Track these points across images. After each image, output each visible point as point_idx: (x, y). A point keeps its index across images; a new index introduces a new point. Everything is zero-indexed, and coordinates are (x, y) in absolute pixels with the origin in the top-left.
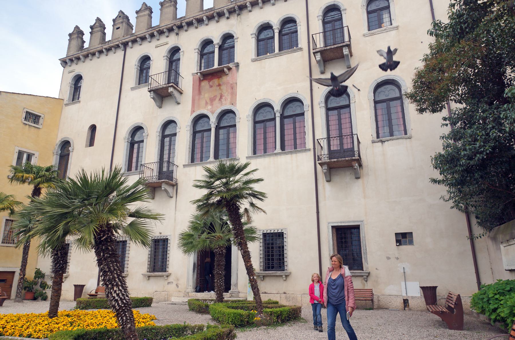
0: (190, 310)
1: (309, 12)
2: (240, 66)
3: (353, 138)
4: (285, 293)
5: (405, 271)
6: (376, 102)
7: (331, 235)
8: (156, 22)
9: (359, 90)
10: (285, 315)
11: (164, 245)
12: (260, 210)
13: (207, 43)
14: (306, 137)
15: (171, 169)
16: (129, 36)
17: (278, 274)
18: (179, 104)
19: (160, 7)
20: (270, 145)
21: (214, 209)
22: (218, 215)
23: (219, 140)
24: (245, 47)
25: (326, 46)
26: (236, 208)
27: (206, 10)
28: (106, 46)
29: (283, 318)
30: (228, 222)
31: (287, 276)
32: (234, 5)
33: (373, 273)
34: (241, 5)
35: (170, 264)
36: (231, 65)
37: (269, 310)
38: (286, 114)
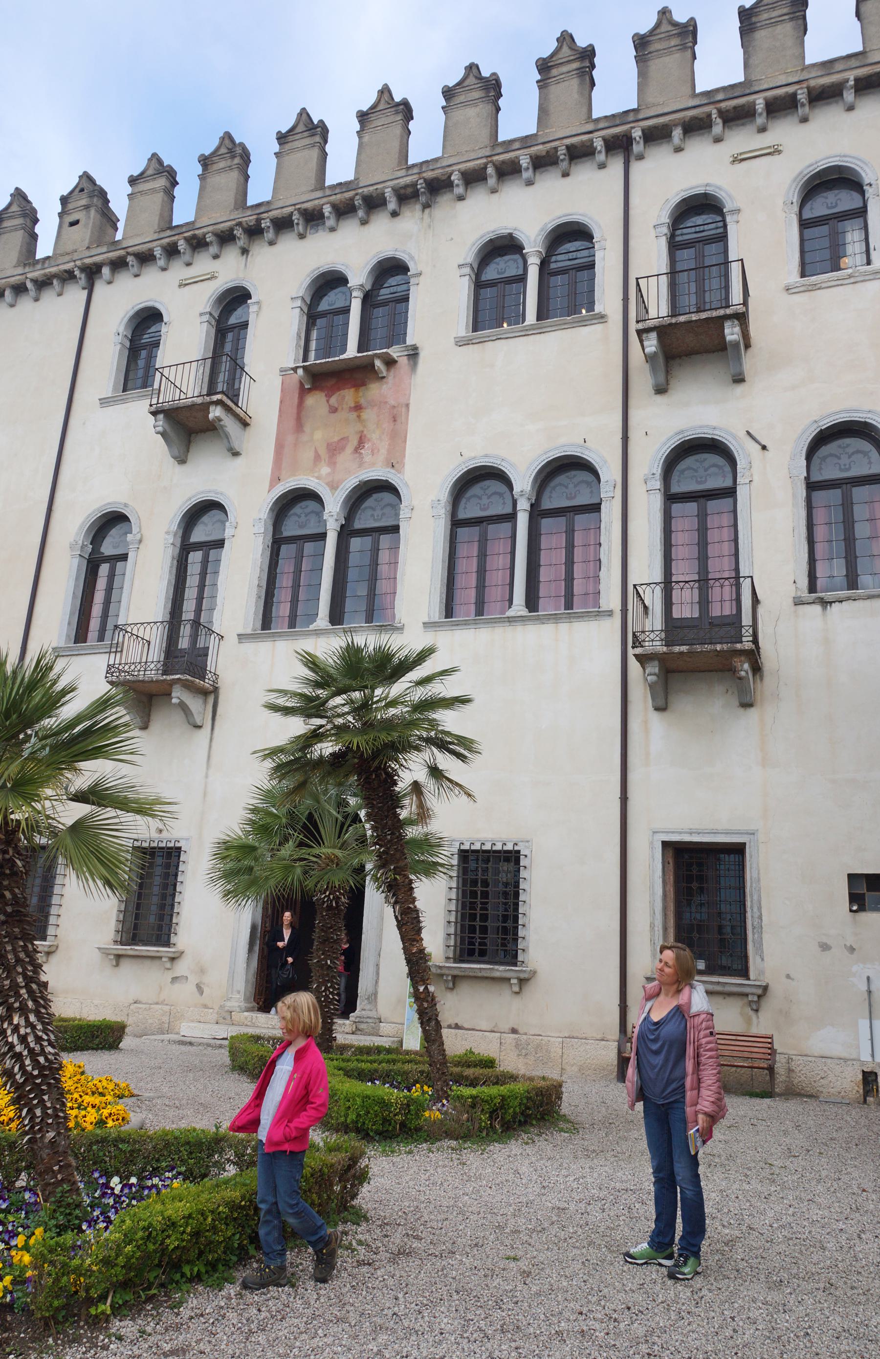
0: (233, 1069)
1: (632, 212)
2: (423, 355)
3: (738, 586)
4: (514, 1031)
5: (873, 988)
6: (812, 486)
7: (659, 866)
8: (184, 211)
9: (764, 448)
10: (514, 1107)
11: (168, 866)
12: (457, 790)
13: (330, 282)
14: (603, 574)
15: (201, 644)
16: (104, 249)
17: (497, 974)
18: (236, 454)
19: (199, 169)
20: (494, 593)
21: (323, 778)
22: (333, 792)
23: (346, 568)
24: (439, 303)
25: (674, 314)
26: (385, 780)
27: (333, 187)
28: (37, 274)
29: (508, 1117)
30: (362, 814)
31: (522, 982)
32: (415, 177)
33: (777, 989)
34: (436, 179)
35: (181, 924)
36: (394, 352)
37: (468, 1091)
38: (546, 504)
